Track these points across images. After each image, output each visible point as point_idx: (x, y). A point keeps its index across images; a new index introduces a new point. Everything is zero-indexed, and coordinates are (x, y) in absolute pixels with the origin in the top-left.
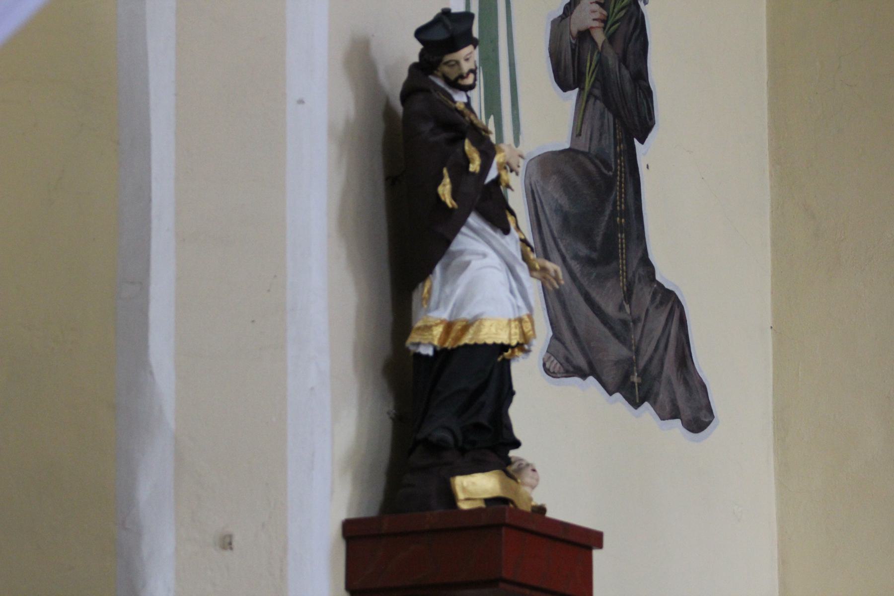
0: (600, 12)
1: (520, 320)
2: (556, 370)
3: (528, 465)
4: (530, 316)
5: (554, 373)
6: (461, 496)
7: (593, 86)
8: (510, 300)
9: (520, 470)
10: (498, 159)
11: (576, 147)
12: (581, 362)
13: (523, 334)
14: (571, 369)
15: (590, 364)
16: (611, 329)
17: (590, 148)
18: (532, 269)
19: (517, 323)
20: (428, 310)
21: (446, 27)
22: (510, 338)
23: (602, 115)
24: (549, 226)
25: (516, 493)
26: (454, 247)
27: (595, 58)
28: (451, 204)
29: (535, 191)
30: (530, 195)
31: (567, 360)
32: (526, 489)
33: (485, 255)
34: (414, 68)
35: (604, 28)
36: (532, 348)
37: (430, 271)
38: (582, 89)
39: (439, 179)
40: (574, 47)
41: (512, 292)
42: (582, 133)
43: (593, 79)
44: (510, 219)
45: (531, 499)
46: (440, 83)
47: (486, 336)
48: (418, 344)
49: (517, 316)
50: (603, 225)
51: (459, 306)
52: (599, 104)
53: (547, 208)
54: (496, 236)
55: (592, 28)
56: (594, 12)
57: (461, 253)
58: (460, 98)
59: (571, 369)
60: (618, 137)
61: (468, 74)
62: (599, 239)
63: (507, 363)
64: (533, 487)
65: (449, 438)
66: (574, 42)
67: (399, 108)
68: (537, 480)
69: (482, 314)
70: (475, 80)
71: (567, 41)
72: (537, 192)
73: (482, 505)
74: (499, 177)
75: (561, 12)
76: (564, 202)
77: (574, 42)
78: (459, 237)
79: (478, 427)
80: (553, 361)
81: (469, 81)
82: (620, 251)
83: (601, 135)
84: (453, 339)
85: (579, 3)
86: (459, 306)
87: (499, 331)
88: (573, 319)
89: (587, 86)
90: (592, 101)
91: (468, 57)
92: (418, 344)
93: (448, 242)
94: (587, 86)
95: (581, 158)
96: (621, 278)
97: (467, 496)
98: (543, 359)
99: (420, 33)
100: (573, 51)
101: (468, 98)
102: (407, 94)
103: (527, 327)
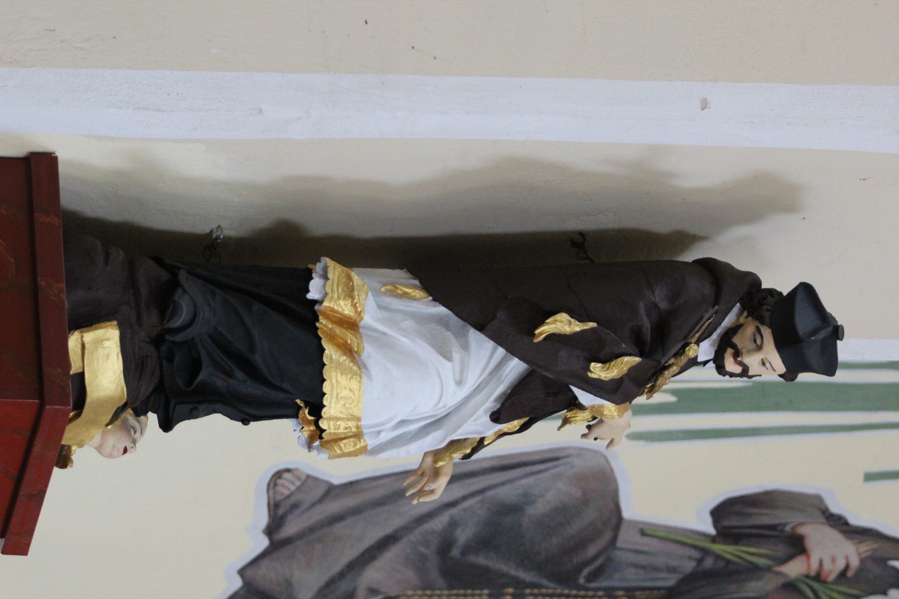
0: (832, 570)
1: (358, 435)
2: (279, 489)
3: (134, 442)
4: (364, 450)
5: (275, 485)
6: (89, 336)
7: (718, 557)
8: (391, 419)
9: (127, 429)
10: (609, 408)
11: (624, 528)
12: (290, 529)
13: (337, 440)
14: (281, 511)
15: (288, 541)
16: (342, 575)
17: (621, 549)
18: (437, 454)
19: (354, 430)
20: (377, 293)
21: (815, 332)
22: (330, 419)
23: (672, 570)
24: (503, 484)
25: (93, 422)
26: (475, 337)
27: (761, 561)
28: (541, 334)
29: (557, 463)
30: (551, 455)
31: (295, 506)
32: (97, 440)
33: (460, 383)
34: (753, 281)
35: (807, 576)
36: (315, 452)
37: (438, 297)
38: (713, 539)
39: (578, 315)
40: (780, 528)
41: (403, 423)
42: (646, 540)
43: (728, 556)
44: (516, 424)
45: (81, 445)
46: (729, 320)
47: (334, 381)
48: (325, 277)
49: (365, 431)
50: (503, 567)
51: (383, 342)
52: (689, 566)
53: (531, 479)
54: (490, 401)
55: (808, 557)
56: (833, 560)
57: (465, 347)
58: (705, 350)
59: (281, 511)
60: (638, 593)
61: (741, 364)
62: (481, 560)
63: (293, 413)
64: (99, 449)
65: (177, 323)
66: (788, 528)
67: (690, 256)
68: (111, 456)
69: (369, 376)
70: (732, 375)
71: (789, 519)
72: (556, 466)
73: (75, 369)
74: (581, 407)
75: (834, 509)
76: (539, 509)
77: (788, 528)
78: (490, 344)
79: (195, 367)
80: (293, 484)
81: (730, 365)
82: (462, 592)
83: (643, 567)
84: (331, 329)
85: (847, 538)
86: (383, 342)
87: (342, 402)
88: (357, 517)
89: (718, 548)
90: (696, 554)
91: (768, 365)
92: (325, 277)
93: (481, 328)
94: (718, 548)
95: (607, 536)
96: (420, 592)
97: (87, 346)
98: (297, 470)
99: (806, 290)
100: (773, 527)
101: (705, 363)
102: (710, 267)
103: (347, 446)
